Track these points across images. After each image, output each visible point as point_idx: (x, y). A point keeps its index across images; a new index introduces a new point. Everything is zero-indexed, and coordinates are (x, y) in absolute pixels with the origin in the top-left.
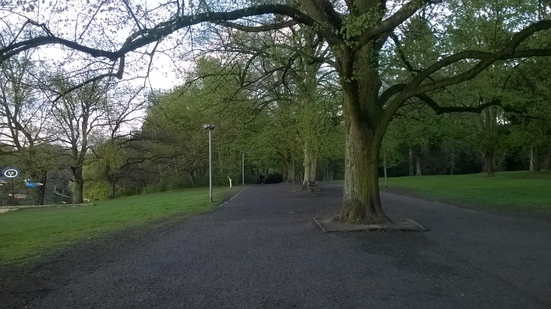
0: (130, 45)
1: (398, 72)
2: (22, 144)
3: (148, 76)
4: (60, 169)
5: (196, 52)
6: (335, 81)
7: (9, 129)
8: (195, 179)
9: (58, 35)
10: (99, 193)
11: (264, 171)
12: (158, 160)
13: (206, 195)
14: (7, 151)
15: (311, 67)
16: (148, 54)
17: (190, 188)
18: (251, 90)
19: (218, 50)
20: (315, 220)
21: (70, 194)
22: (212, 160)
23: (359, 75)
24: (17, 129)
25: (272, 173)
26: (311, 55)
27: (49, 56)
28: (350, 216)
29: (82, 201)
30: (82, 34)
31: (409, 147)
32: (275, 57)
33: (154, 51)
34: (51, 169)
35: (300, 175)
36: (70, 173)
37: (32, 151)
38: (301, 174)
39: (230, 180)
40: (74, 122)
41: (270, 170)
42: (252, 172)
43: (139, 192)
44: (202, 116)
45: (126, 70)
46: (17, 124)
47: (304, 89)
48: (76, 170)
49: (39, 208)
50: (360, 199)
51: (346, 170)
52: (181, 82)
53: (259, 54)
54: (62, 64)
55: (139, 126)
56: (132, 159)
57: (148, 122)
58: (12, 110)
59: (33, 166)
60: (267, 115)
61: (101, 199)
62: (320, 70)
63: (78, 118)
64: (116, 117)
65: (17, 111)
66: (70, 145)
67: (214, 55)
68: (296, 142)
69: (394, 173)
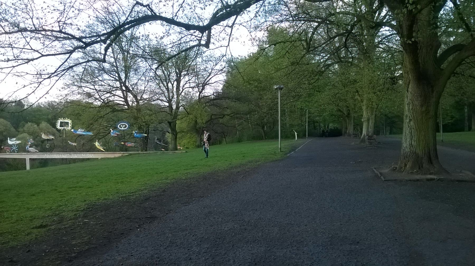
0: (216, 19)
1: (457, 35)
2: (130, 103)
3: (228, 45)
4: (160, 123)
5: (268, 23)
6: (396, 42)
7: (120, 91)
8: (266, 132)
9: (160, 14)
10: (189, 142)
11: (325, 126)
12: (235, 116)
13: (275, 146)
14: (119, 109)
15: (372, 31)
16: (229, 26)
17: (261, 140)
18: (315, 55)
19: (287, 20)
20: (374, 170)
21: (167, 143)
22: (281, 116)
23: (420, 36)
24: (127, 92)
25: (333, 128)
26: (372, 20)
27: (152, 32)
28: (408, 166)
29: (176, 149)
30: (177, 12)
31: (465, 104)
32: (338, 25)
33: (233, 24)
34: (152, 123)
35: (358, 130)
36: (166, 126)
37: (138, 109)
38: (359, 129)
39: (296, 134)
40: (170, 85)
41: (331, 125)
42: (314, 127)
43: (220, 143)
44: (272, 78)
45: (212, 40)
46: (127, 87)
47: (364, 51)
48: (172, 125)
49: (144, 154)
50: (418, 151)
51: (404, 125)
52: (255, 49)
53: (324, 22)
54: (162, 38)
55: (220, 87)
56: (215, 115)
57: (227, 85)
58: (123, 76)
59: (139, 121)
60: (329, 77)
61: (190, 147)
62: (380, 34)
63: (172, 83)
64: (202, 80)
65: (126, 77)
66: (167, 104)
67: (285, 25)
68: (355, 100)
69: (448, 129)
